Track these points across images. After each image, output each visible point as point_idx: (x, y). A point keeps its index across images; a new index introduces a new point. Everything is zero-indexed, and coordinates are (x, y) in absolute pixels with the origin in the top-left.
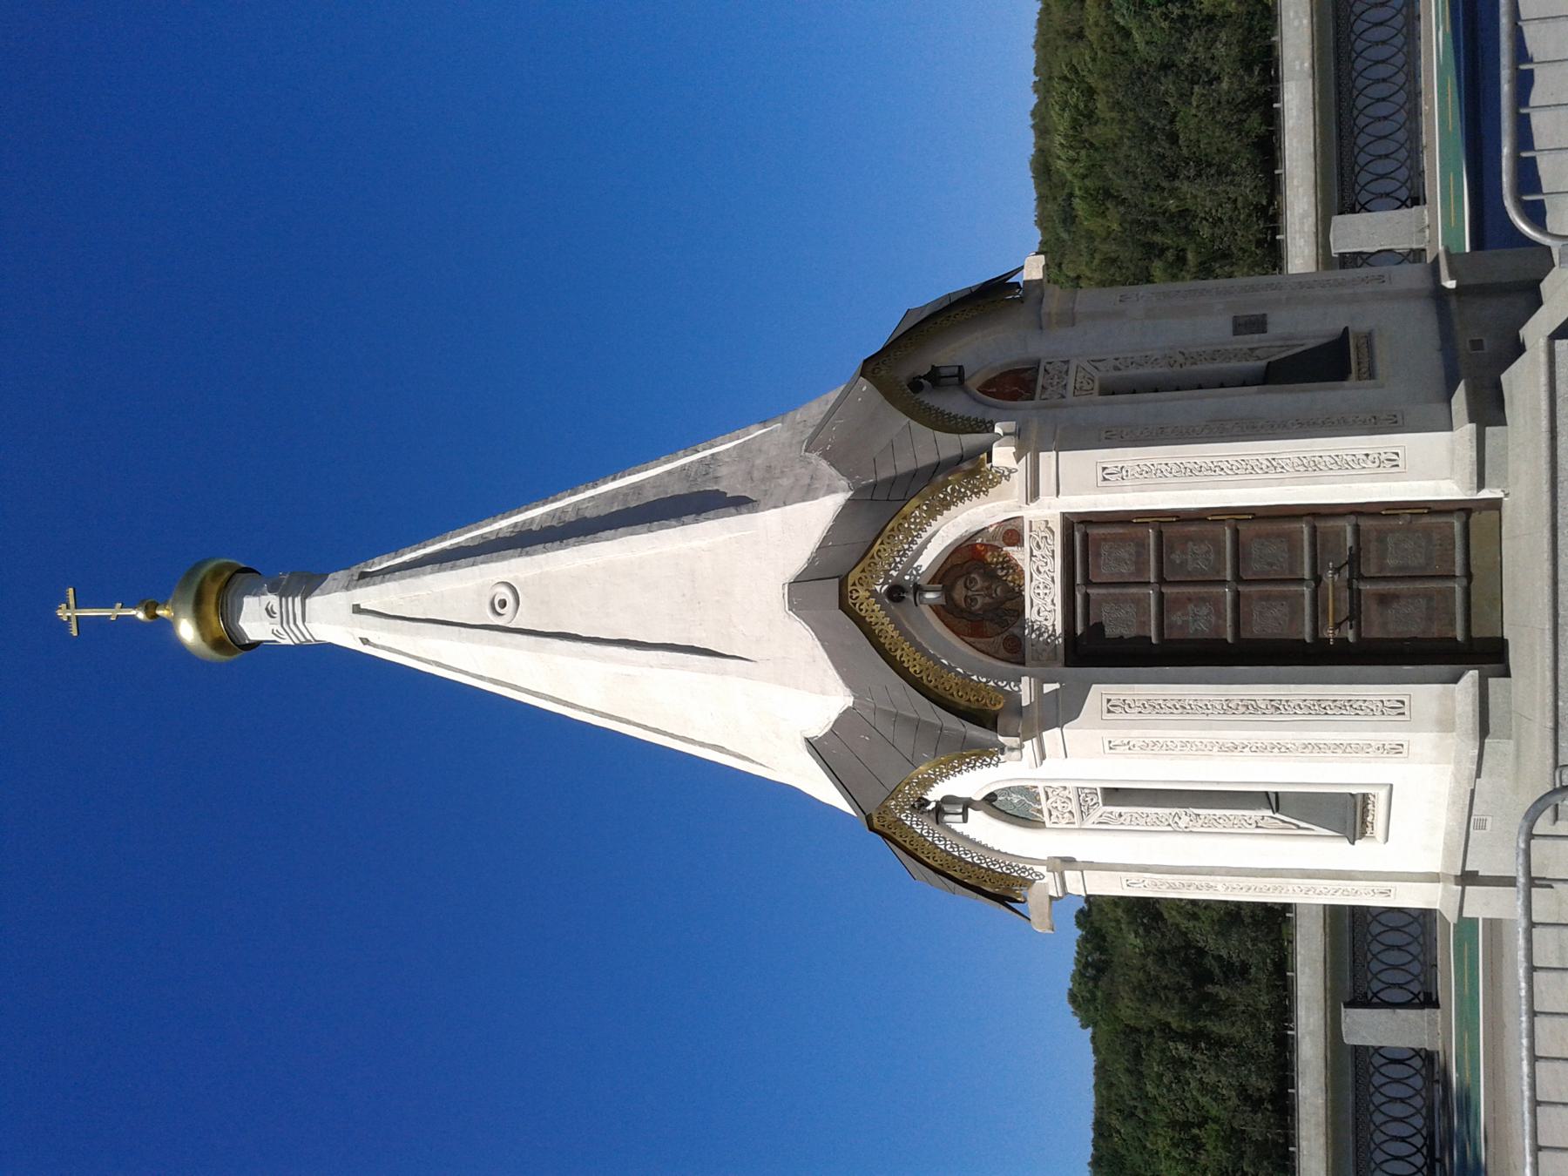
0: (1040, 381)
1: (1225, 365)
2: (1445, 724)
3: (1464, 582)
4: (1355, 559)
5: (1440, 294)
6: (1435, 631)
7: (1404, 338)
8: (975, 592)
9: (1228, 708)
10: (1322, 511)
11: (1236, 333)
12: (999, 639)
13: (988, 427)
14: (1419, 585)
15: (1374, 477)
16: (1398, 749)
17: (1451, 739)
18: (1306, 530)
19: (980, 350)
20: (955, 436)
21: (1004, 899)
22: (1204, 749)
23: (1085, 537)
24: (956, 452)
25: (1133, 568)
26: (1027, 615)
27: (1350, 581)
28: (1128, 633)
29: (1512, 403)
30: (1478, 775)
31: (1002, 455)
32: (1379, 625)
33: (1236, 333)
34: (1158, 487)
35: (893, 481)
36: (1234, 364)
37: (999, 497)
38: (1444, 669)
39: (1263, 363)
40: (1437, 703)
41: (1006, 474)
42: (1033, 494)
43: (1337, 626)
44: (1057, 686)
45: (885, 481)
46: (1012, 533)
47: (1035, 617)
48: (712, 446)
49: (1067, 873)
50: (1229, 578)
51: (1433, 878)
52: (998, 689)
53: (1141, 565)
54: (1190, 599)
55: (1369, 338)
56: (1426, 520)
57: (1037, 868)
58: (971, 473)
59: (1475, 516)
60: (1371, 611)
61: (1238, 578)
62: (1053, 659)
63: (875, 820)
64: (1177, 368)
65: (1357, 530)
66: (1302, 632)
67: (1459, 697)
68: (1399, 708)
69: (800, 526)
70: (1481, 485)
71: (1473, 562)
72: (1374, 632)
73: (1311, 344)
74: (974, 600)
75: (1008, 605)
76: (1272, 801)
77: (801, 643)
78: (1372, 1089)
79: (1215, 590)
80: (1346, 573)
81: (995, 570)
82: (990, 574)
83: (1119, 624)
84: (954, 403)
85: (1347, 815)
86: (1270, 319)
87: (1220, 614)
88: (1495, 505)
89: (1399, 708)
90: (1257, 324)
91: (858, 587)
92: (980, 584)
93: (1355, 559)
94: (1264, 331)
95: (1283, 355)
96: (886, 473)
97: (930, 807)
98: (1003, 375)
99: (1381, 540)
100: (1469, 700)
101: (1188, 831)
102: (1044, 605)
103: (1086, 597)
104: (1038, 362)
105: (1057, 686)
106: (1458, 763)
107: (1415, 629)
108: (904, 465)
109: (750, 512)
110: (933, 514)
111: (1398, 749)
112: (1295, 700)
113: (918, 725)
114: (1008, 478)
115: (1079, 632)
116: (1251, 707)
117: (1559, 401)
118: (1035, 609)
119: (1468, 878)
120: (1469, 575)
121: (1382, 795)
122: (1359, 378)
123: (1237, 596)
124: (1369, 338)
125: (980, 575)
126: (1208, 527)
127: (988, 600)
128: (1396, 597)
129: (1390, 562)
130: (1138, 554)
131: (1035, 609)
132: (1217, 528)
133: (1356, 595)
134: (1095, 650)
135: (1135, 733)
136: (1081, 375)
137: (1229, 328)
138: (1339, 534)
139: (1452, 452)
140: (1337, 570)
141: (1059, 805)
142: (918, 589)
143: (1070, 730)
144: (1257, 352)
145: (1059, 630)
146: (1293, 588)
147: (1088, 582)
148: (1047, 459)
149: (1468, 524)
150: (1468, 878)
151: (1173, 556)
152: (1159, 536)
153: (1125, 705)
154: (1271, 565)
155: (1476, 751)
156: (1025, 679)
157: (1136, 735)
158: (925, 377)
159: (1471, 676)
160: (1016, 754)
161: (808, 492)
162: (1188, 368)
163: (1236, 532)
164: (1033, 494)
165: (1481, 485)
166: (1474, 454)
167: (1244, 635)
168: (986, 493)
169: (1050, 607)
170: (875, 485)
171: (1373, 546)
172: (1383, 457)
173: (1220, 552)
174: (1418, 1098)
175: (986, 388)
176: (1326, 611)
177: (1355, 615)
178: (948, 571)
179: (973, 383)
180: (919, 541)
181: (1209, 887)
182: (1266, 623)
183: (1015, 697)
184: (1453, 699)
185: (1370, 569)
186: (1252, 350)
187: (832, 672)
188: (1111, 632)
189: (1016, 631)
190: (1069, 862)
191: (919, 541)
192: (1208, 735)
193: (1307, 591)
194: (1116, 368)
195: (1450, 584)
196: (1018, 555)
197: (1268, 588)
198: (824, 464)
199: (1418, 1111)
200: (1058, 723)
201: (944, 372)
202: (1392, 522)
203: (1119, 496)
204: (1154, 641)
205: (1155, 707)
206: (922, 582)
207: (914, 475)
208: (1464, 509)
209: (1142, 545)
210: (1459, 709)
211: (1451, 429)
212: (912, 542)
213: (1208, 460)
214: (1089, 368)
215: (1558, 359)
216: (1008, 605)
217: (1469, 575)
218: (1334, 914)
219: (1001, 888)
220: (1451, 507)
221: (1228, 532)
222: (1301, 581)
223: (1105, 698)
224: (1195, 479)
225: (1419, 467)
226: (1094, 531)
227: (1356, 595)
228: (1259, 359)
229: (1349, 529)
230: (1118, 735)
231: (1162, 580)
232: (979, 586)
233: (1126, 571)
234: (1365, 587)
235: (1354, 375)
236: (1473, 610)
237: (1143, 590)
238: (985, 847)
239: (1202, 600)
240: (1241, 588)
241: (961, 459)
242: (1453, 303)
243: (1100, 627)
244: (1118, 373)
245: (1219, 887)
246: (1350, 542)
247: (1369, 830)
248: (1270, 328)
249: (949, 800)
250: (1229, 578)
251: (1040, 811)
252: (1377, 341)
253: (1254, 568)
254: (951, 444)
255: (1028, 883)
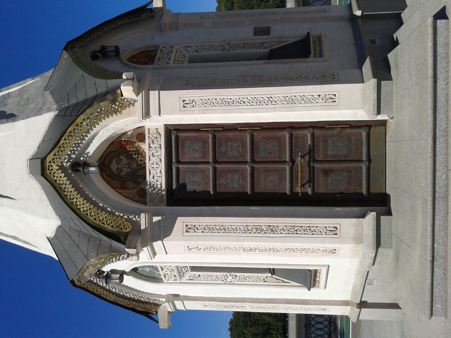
0: (158, 55)
1: (249, 51)
2: (358, 240)
3: (367, 163)
4: (312, 151)
5: (353, 18)
6: (352, 189)
7: (337, 40)
8: (119, 165)
9: (247, 230)
10: (296, 126)
11: (255, 34)
12: (135, 191)
13: (119, 76)
14: (345, 165)
15: (323, 108)
16: (333, 251)
17: (361, 248)
18: (287, 136)
19: (129, 40)
20: (104, 81)
21: (147, 314)
22: (235, 250)
23: (177, 137)
24: (105, 90)
25: (201, 155)
26: (148, 179)
27: (309, 162)
28: (199, 189)
29: (397, 67)
30: (373, 264)
31: (127, 91)
32: (324, 186)
33: (255, 34)
34: (212, 111)
35: (75, 105)
36: (254, 50)
37: (129, 115)
38: (356, 209)
39: (268, 50)
40: (354, 229)
41: (131, 103)
42: (147, 114)
43: (303, 186)
44: (160, 218)
45: (72, 105)
46: (140, 135)
47: (151, 179)
48: (9, 89)
49: (176, 302)
50: (249, 160)
51: (346, 303)
52: (128, 220)
53: (205, 154)
54: (229, 171)
55: (319, 38)
56: (348, 131)
57: (161, 299)
58: (112, 101)
59: (373, 129)
60: (320, 179)
61: (253, 161)
62: (160, 202)
63: (76, 283)
64: (226, 51)
65: (313, 135)
66: (285, 189)
67: (365, 226)
68: (334, 231)
69: (33, 130)
70: (379, 112)
71: (372, 153)
72: (321, 189)
73: (291, 41)
74: (121, 170)
75: (140, 173)
76: (273, 271)
77: (35, 192)
78: (311, 326)
79: (242, 166)
80: (307, 158)
81: (132, 154)
82: (129, 156)
83: (195, 183)
84: (111, 65)
85: (308, 278)
86: (272, 29)
87: (244, 179)
88: (384, 123)
89: (334, 231)
90: (266, 31)
91: (52, 164)
92: (125, 161)
93: (312, 151)
94: (269, 35)
95: (278, 46)
96: (73, 101)
97: (105, 274)
98: (141, 53)
99: (325, 141)
100: (371, 227)
101: (231, 284)
102: (156, 174)
103: (178, 169)
104: (159, 46)
105: (160, 218)
106: (364, 258)
107: (342, 188)
108: (81, 97)
109: (13, 121)
110: (92, 125)
111: (333, 251)
112: (281, 226)
113: (90, 237)
114: (133, 105)
115: (174, 188)
116: (259, 230)
117: (438, 58)
118: (152, 176)
119: (363, 305)
120: (369, 160)
121: (324, 270)
122: (315, 57)
123: (253, 169)
124: (319, 38)
125: (122, 159)
126: (237, 133)
127: (128, 170)
128: (332, 171)
129: (330, 152)
130: (204, 147)
131: (152, 176)
132: (243, 134)
133: (312, 170)
134: (182, 198)
135: (200, 243)
136: (178, 54)
137: (252, 32)
138: (304, 138)
139: (364, 94)
140: (303, 157)
141: (168, 272)
142: (86, 165)
143: (167, 241)
144: (265, 45)
145: (164, 187)
146: (281, 166)
147: (178, 162)
148: (153, 94)
149: (369, 134)
150: (363, 305)
151: (221, 149)
152: (214, 137)
153: (195, 228)
154: (269, 153)
155: (374, 255)
156: (143, 215)
157: (201, 244)
158: (99, 52)
159: (371, 216)
160: (135, 258)
161: (39, 112)
162: (231, 52)
163: (252, 136)
164: (147, 114)
165: (379, 112)
166: (376, 95)
167: (257, 190)
168: (121, 112)
169: (159, 175)
170: (67, 108)
171: (321, 144)
172: (328, 97)
173: (244, 146)
174: (326, 335)
175: (130, 60)
176: (297, 178)
177: (311, 181)
178: (108, 154)
179: (124, 56)
180: (87, 139)
181: (242, 307)
182: (267, 184)
183: (137, 224)
184: (362, 227)
185: (320, 157)
186: (263, 43)
187: (50, 207)
188: (190, 188)
189: (143, 186)
190: (176, 296)
191: (87, 139)
192: (238, 244)
193: (288, 168)
194: (197, 51)
195: (360, 164)
196: (144, 146)
197: (268, 166)
198: (50, 97)
199: (326, 333)
200: (160, 238)
201: (109, 49)
202: (331, 132)
203: (192, 116)
204: (211, 193)
205: (211, 229)
206: (89, 161)
207: (85, 102)
208: (367, 125)
209: (205, 142)
210: (365, 232)
211: (363, 82)
212: (83, 139)
213: (237, 98)
214: (183, 50)
215: (439, 32)
216: (140, 173)
217: (369, 160)
218: (299, 317)
219: (145, 309)
220: (359, 124)
221: (248, 136)
222: (285, 162)
223: (185, 224)
224: (230, 107)
225: (344, 103)
226: (181, 135)
227: (312, 170)
228: (266, 48)
229: (309, 135)
230: (192, 244)
231: (215, 161)
232: (124, 162)
233: (197, 156)
234: (317, 166)
235: (312, 55)
236: (372, 178)
237: (206, 166)
238: (136, 290)
239: (236, 171)
240: (254, 166)
241: (107, 93)
242: (360, 22)
243: (184, 185)
244: (197, 54)
245: (247, 307)
246: (309, 142)
247: (317, 284)
248: (271, 33)
249: (113, 271)
250: (249, 160)
251: (160, 275)
252: (323, 39)
253: (261, 155)
254: (103, 85)
255: (157, 305)
